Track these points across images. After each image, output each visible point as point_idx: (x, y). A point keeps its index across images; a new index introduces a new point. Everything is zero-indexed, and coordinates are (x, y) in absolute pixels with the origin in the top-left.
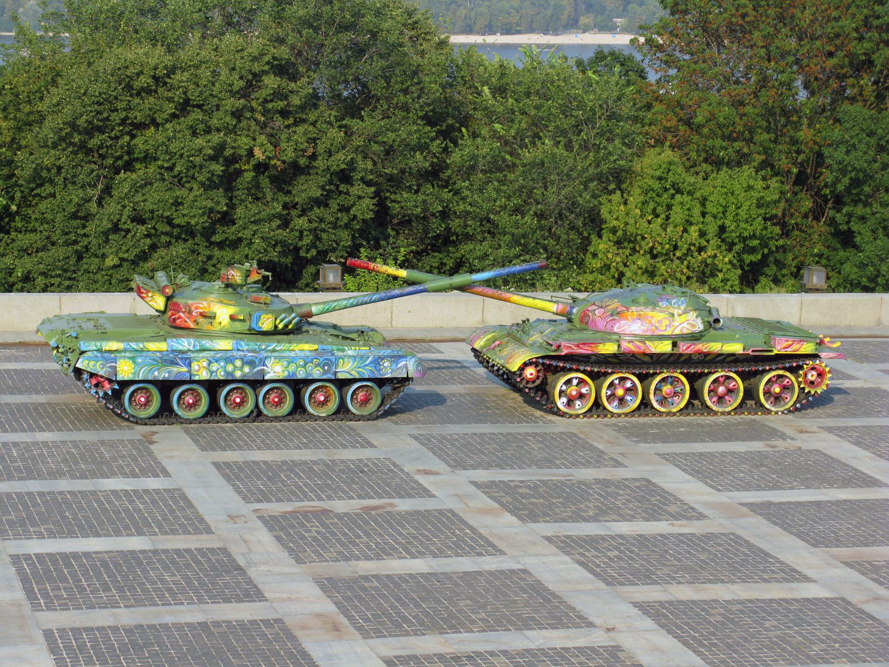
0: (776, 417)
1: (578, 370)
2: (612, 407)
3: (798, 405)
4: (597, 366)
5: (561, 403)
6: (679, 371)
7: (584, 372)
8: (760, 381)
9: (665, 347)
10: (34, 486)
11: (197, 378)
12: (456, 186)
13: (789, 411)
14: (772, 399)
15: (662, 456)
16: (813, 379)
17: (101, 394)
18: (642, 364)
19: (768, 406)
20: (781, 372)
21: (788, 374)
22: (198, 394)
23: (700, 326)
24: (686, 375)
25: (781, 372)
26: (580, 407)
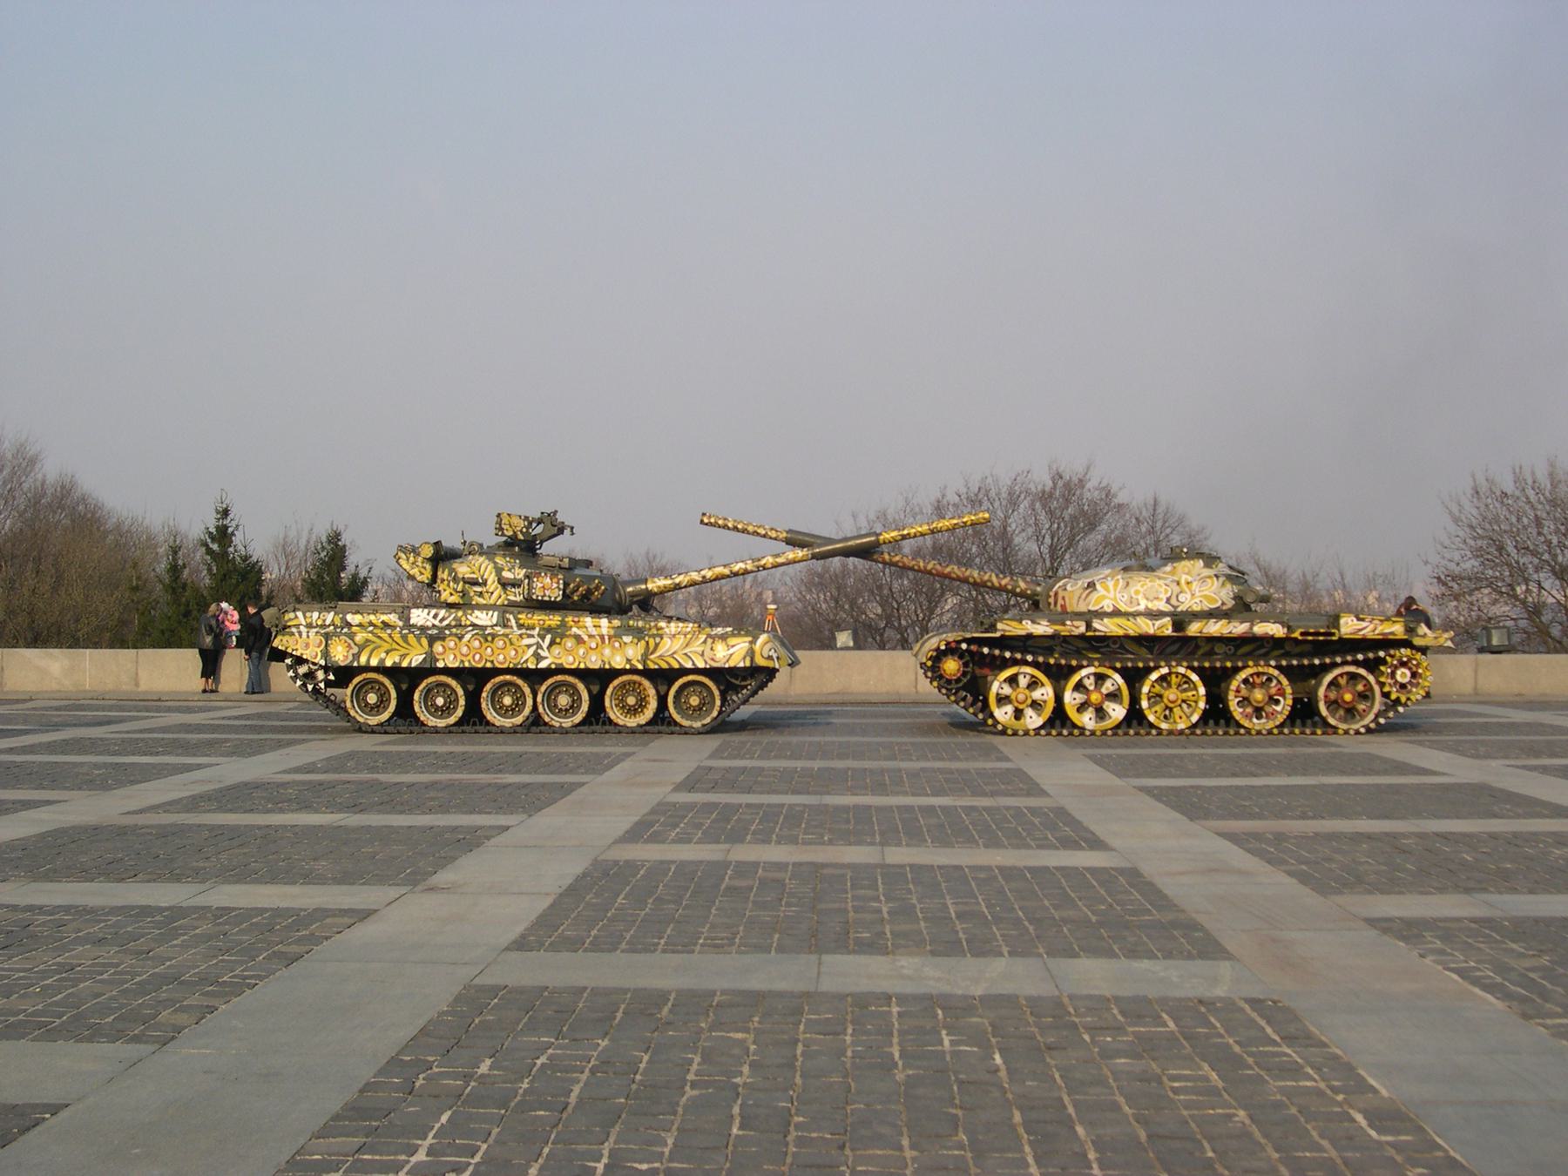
0: (1349, 739)
1: (1345, 663)
2: (1087, 720)
3: (1382, 721)
4: (1059, 657)
5: (1003, 714)
6: (1273, 663)
7: (1356, 663)
8: (1319, 684)
9: (1165, 628)
10: (799, 764)
11: (440, 665)
12: (1474, 522)
13: (1369, 731)
14: (1342, 712)
15: (1141, 789)
16: (1405, 680)
17: (310, 687)
18: (1134, 656)
19: (1332, 721)
20: (1352, 669)
21: (1362, 671)
22: (518, 687)
23: (1230, 603)
24: (1200, 671)
25: (1352, 669)
26: (1033, 720)
